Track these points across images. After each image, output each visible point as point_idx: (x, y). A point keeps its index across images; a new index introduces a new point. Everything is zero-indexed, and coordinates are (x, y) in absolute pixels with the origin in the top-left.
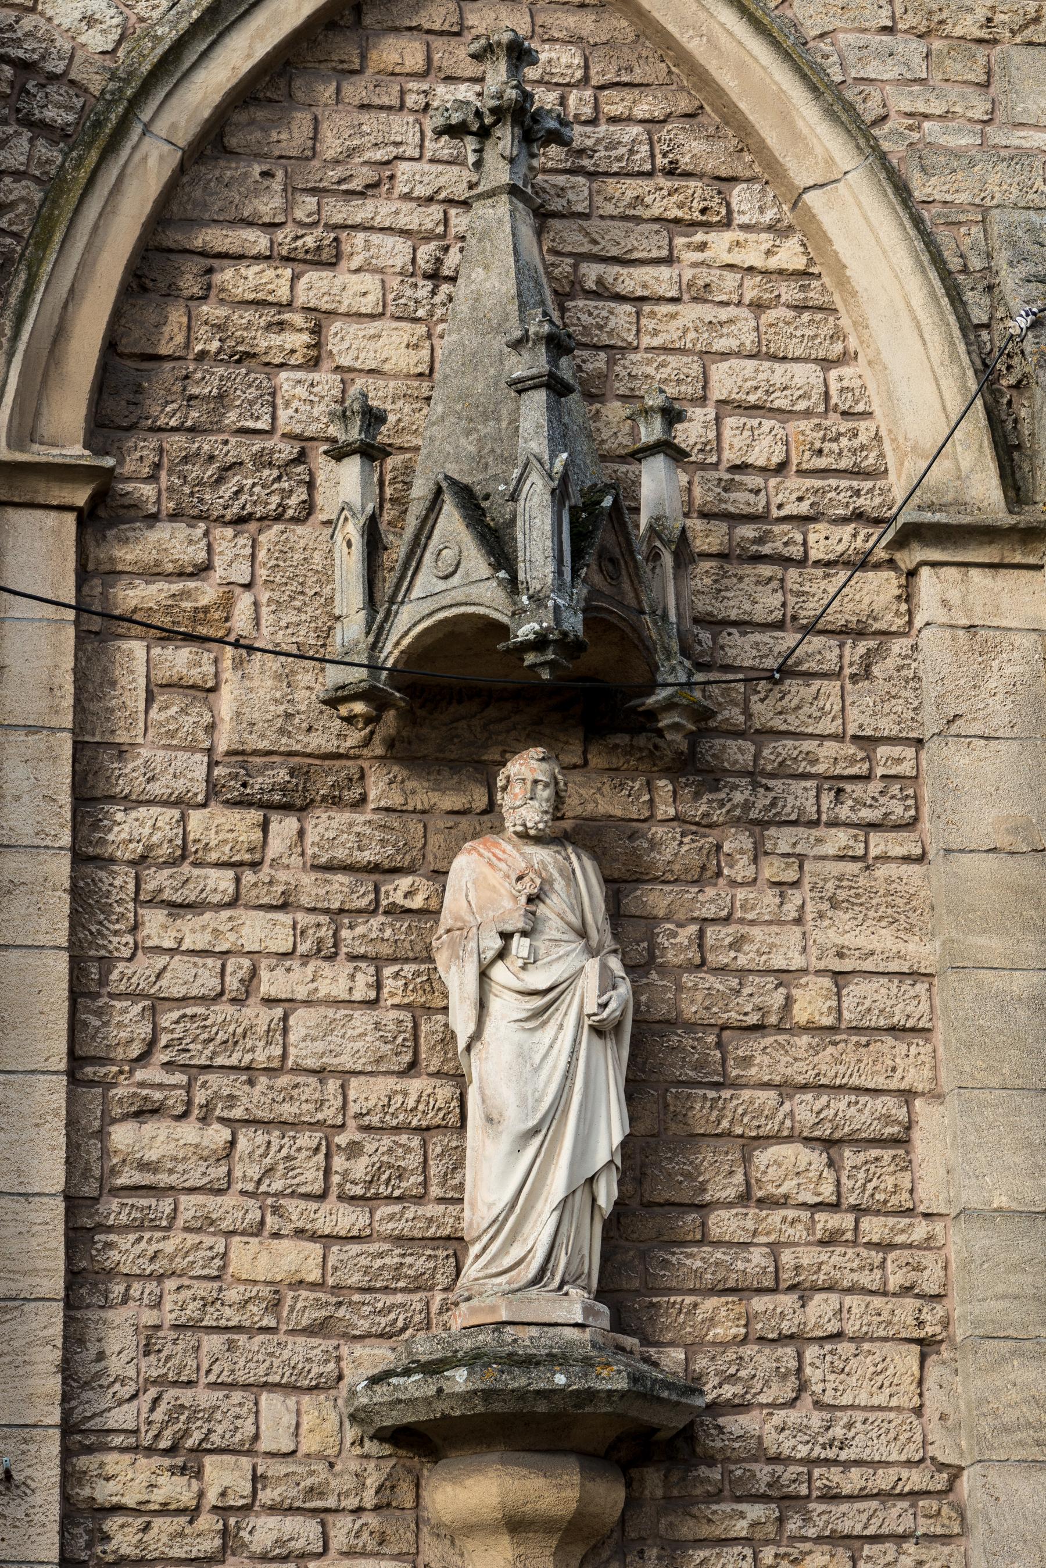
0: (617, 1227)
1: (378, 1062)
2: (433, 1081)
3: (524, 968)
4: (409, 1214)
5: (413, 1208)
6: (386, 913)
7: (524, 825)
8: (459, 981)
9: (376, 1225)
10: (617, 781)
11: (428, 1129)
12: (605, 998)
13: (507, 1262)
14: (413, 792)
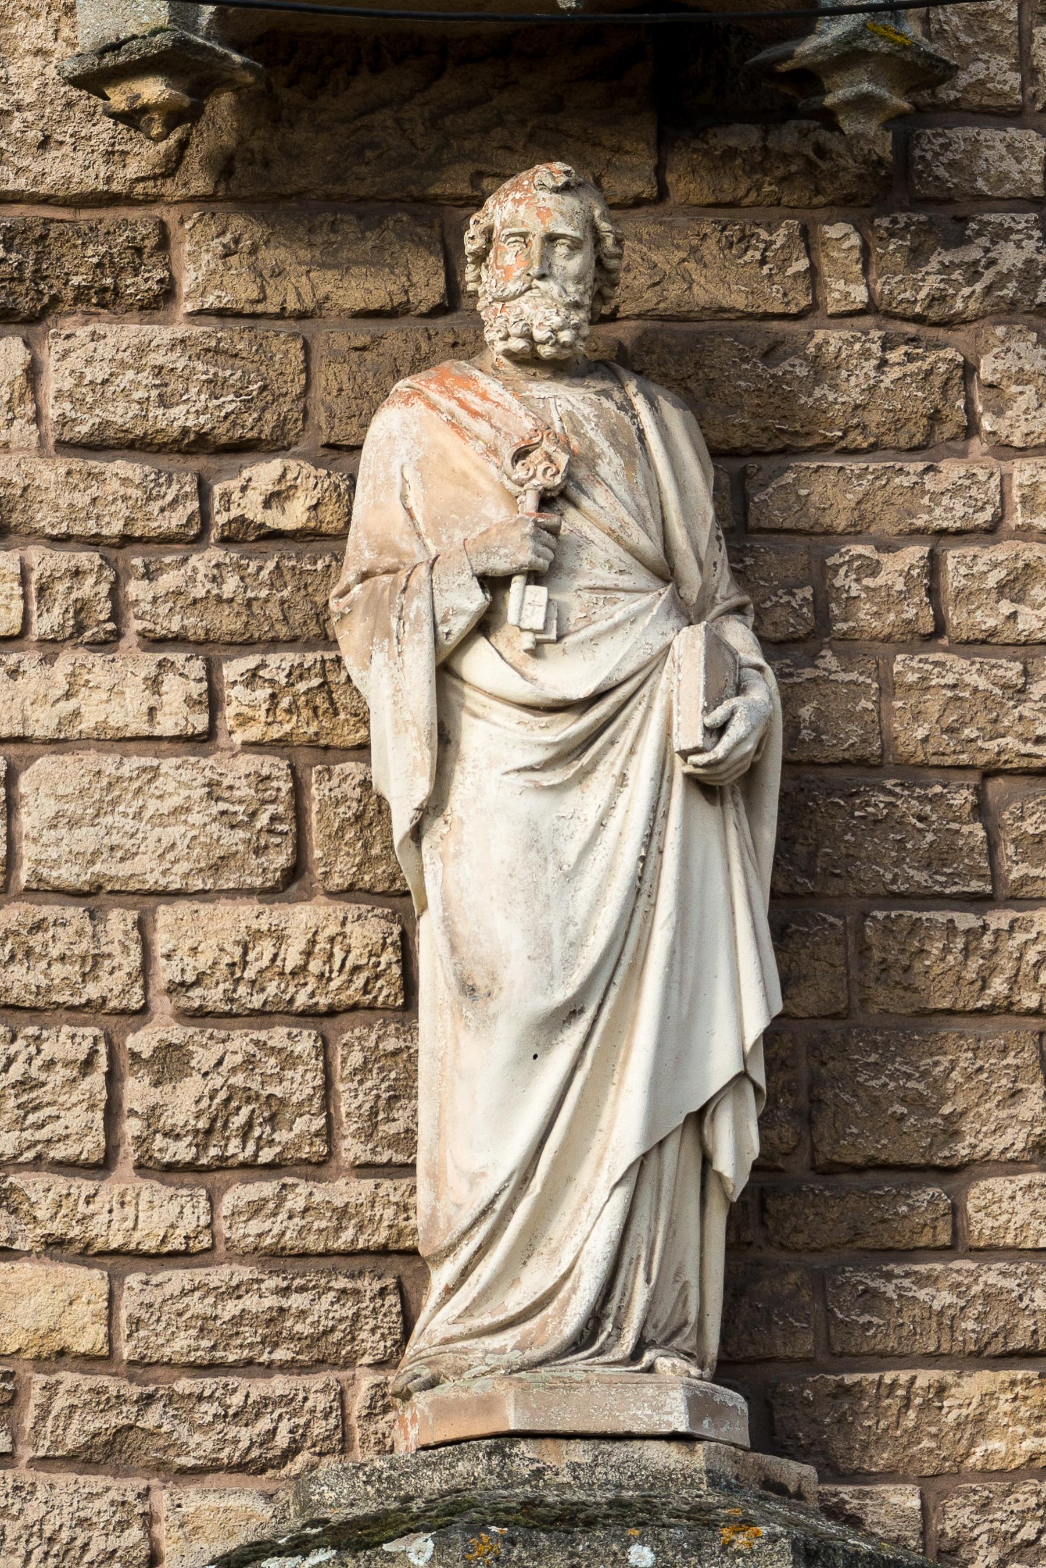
0: (757, 1218)
1: (216, 868)
2: (340, 909)
3: (536, 652)
4: (296, 1202)
5: (303, 1188)
6: (225, 541)
7: (528, 336)
8: (392, 686)
9: (222, 1226)
11: (332, 1012)
12: (719, 714)
13: (515, 1301)
14: (278, 273)
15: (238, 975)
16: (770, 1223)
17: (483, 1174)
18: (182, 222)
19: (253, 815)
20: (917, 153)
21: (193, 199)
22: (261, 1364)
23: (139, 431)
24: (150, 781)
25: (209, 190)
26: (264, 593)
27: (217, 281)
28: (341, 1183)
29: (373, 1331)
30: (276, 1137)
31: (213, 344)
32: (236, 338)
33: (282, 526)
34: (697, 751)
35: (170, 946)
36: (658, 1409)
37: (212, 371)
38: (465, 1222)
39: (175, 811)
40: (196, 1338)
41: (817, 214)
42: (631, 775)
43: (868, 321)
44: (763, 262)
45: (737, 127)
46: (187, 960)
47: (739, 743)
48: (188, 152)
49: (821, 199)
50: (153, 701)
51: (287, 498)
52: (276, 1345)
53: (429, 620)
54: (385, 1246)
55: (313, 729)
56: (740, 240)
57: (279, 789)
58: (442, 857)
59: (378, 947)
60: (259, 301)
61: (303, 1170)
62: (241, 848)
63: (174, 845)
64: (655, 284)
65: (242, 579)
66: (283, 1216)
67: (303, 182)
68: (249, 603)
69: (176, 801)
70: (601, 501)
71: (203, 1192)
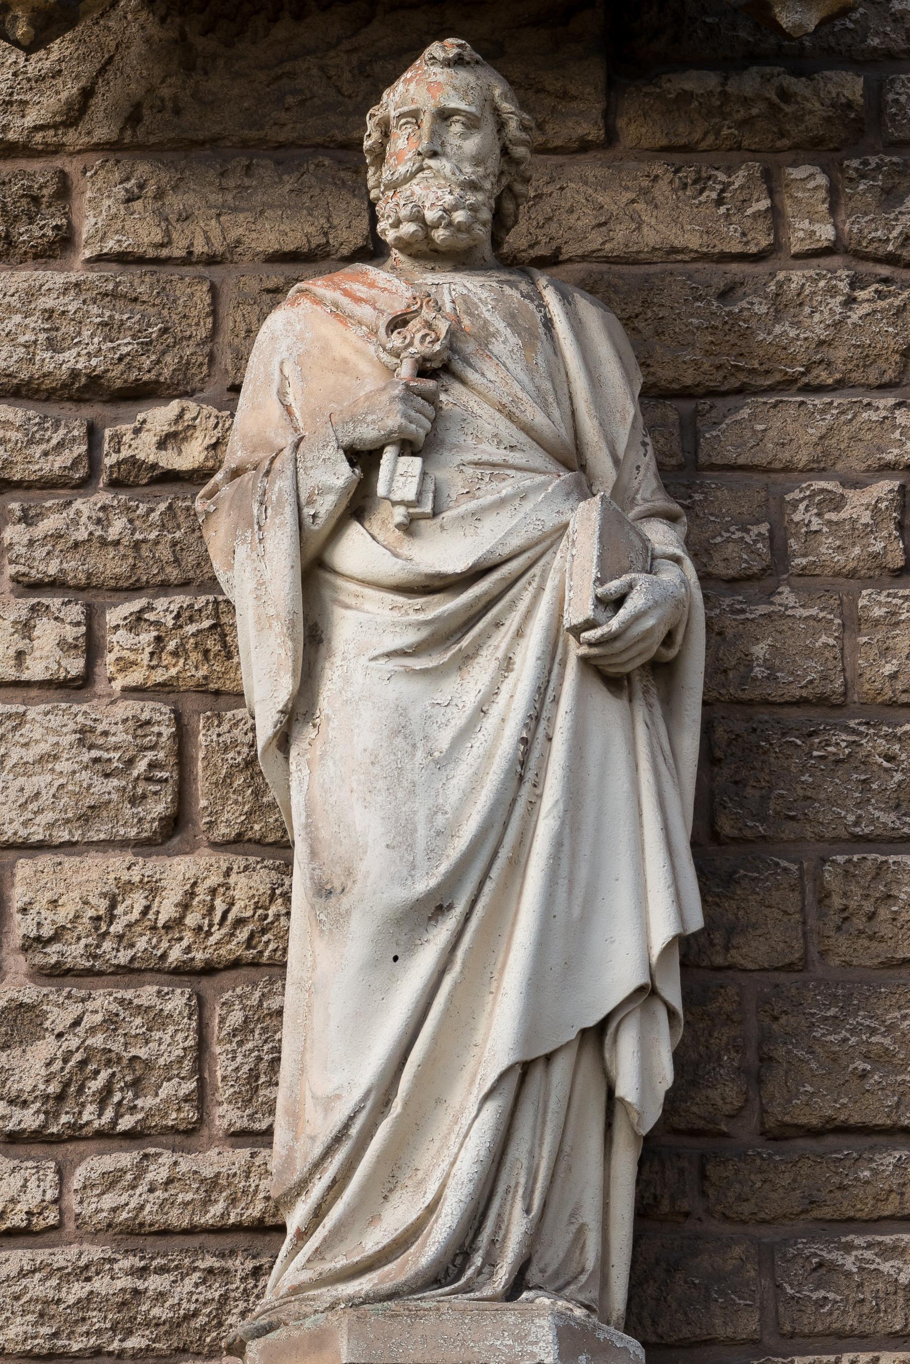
0: (681, 1164)
1: (85, 819)
2: (223, 860)
3: (409, 528)
4: (158, 1172)
5: (167, 1158)
6: (115, 484)
7: (418, 218)
8: (257, 577)
9: (72, 1201)
10: (689, 173)
11: (209, 970)
12: (614, 586)
13: (375, 1239)
14: (185, 217)
15: (104, 928)
16: (711, 1192)
17: (338, 1097)
18: (84, 172)
19: (131, 762)
20: (891, 96)
21: (96, 148)
22: (110, 1354)
23: (24, 375)
24: (15, 729)
25: (114, 137)
26: (153, 536)
27: (119, 225)
28: (212, 1153)
29: (243, 1314)
30: (139, 1103)
31: (111, 286)
32: (137, 281)
33: (176, 466)
34: (590, 624)
35: (26, 899)
36: (520, 1338)
37: (108, 314)
38: (317, 1150)
39: (41, 759)
40: (35, 1324)
41: (781, 157)
42: (517, 660)
43: (836, 261)
44: (720, 202)
45: (694, 73)
46: (44, 913)
47: (637, 617)
48: (93, 102)
49: (786, 142)
50: (22, 645)
51: (185, 439)
52: (130, 1333)
53: (292, 500)
54: (261, 1220)
55: (203, 671)
56: (695, 182)
57: (159, 734)
58: (309, 763)
59: (265, 899)
60: (162, 245)
61: (170, 1139)
62: (114, 796)
63: (38, 794)
64: (600, 225)
65: (131, 521)
66: (142, 1188)
67: (217, 129)
68: (137, 545)
69: (44, 748)
70: (490, 375)
71: (52, 1164)
